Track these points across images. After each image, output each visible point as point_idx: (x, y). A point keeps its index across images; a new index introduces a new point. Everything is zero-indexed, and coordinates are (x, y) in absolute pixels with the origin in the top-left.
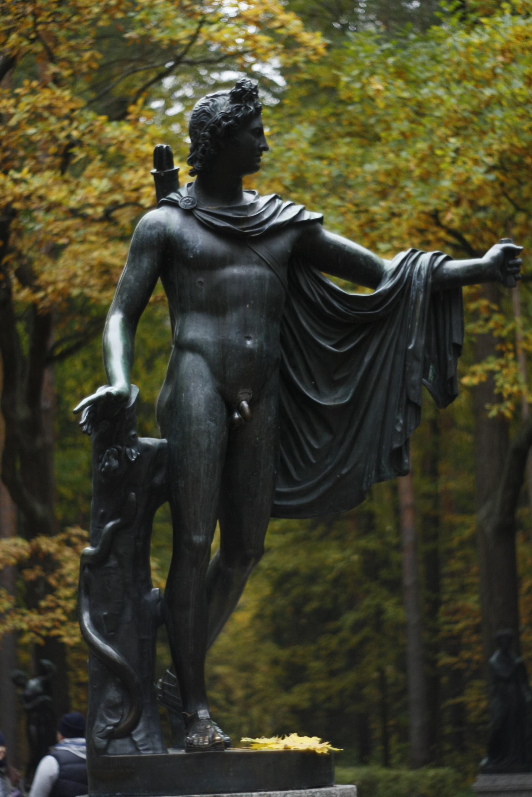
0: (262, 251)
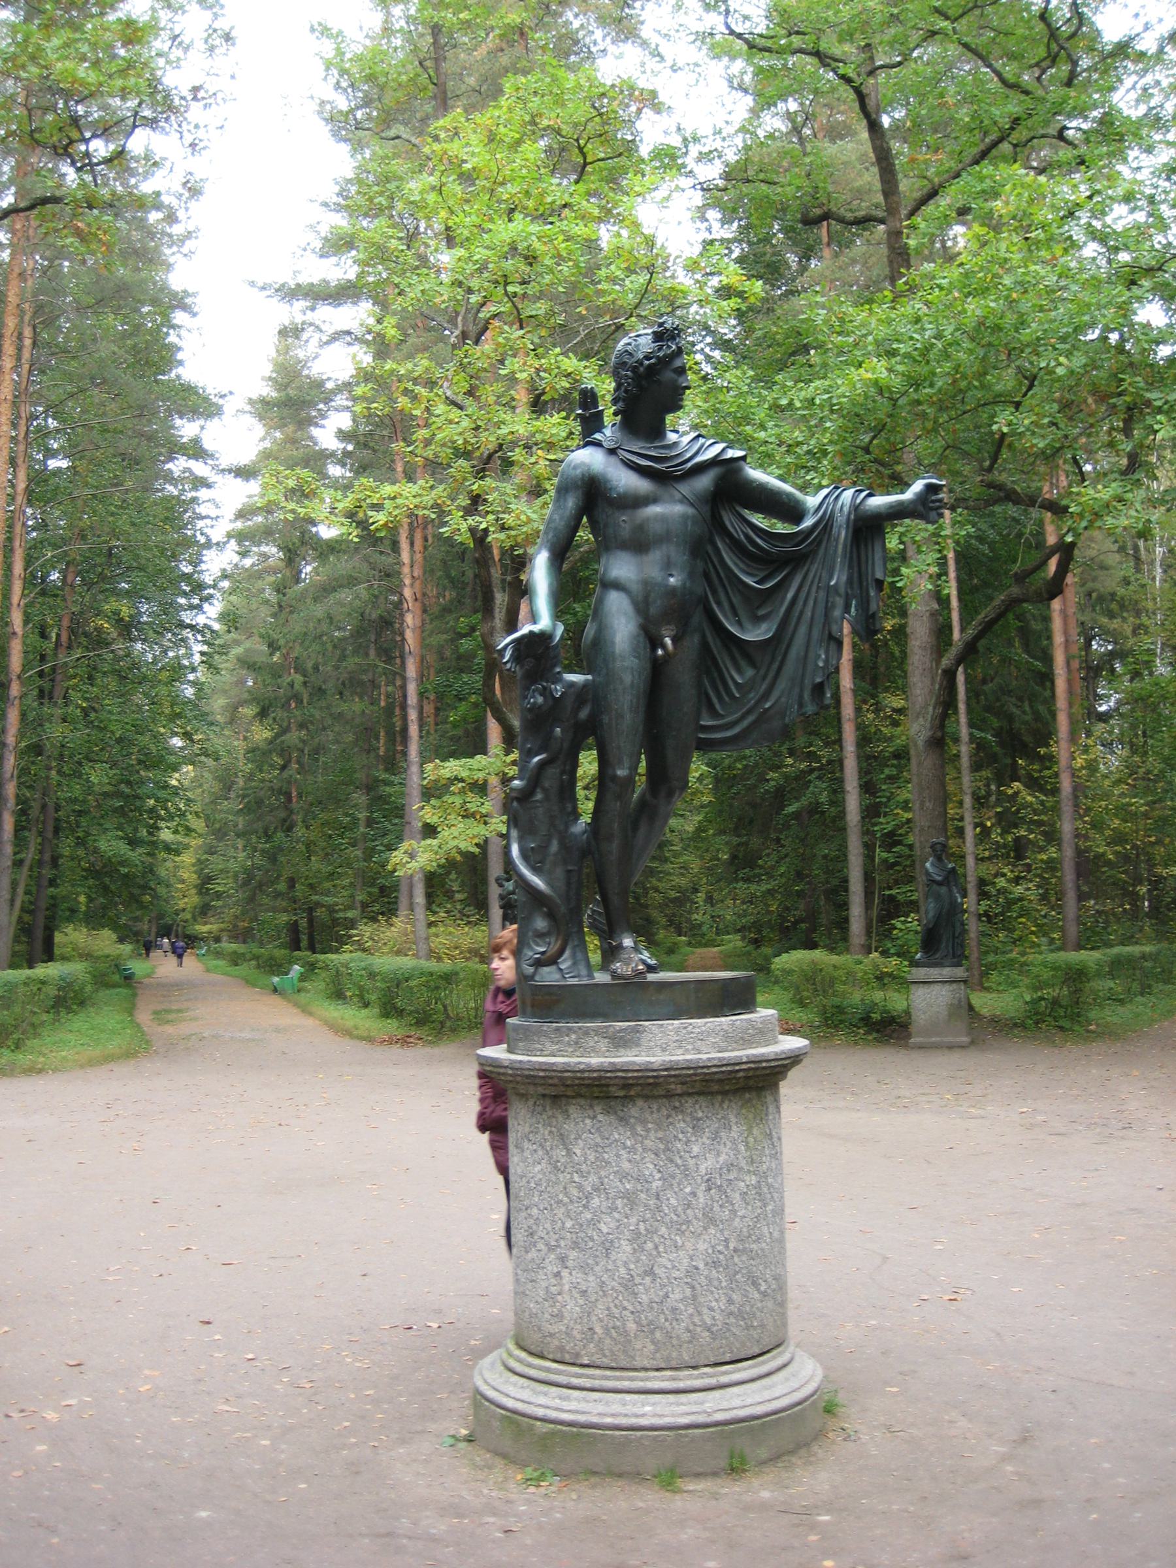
0: (685, 488)
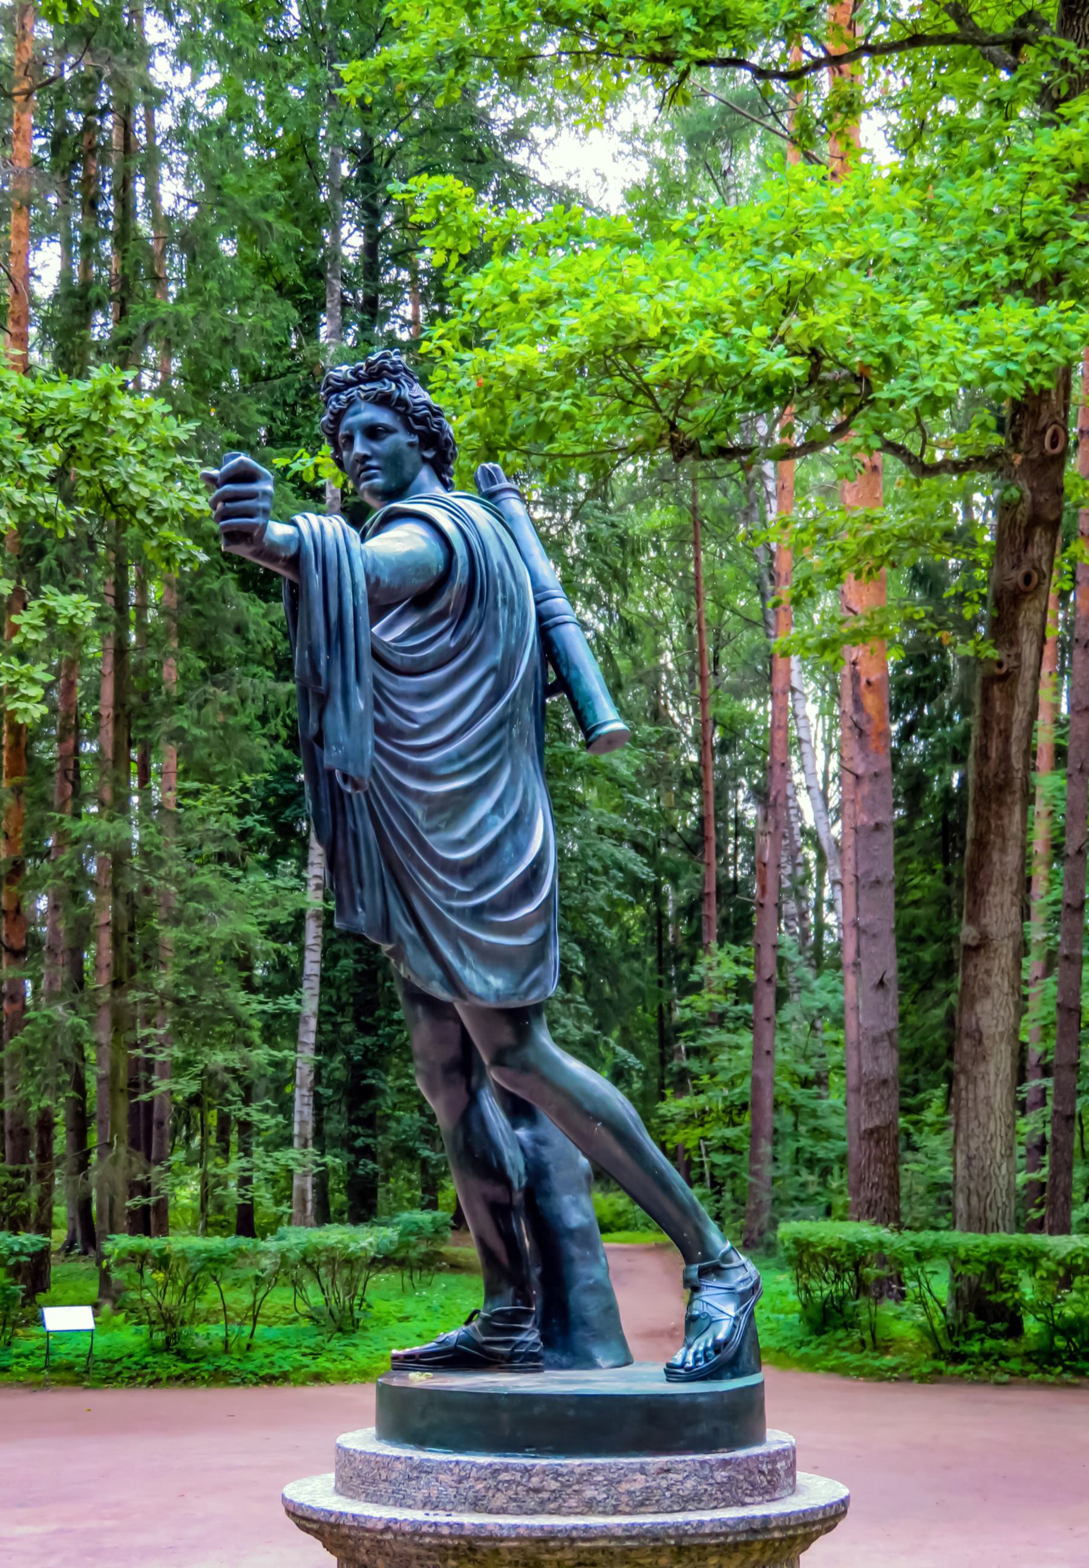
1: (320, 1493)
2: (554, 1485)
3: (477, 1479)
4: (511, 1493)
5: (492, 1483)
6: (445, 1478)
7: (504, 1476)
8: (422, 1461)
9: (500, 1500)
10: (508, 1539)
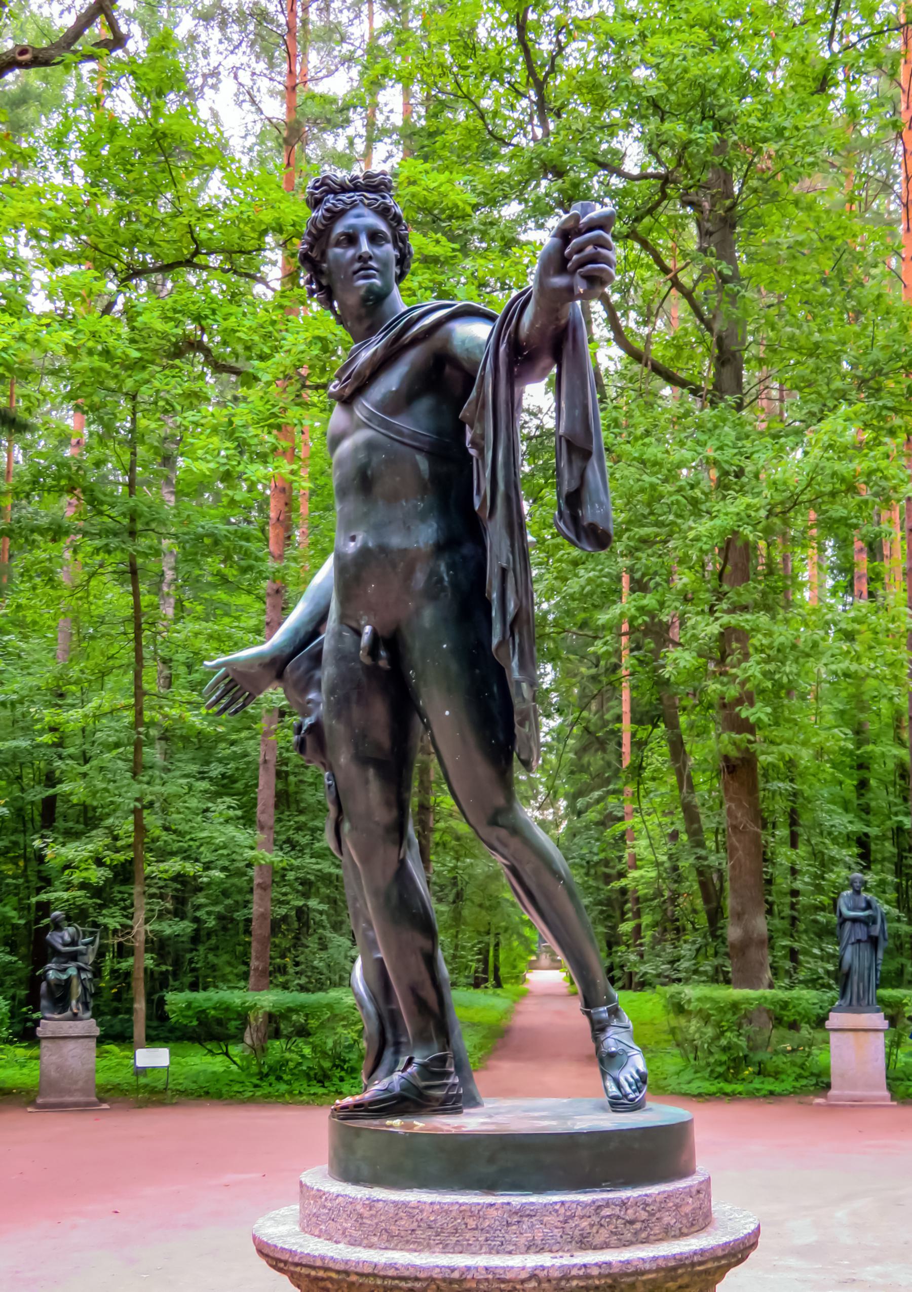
0: (365, 406)
1: (284, 1228)
2: (644, 1215)
3: (582, 1217)
4: (612, 1227)
5: (595, 1219)
6: (551, 1219)
7: (606, 1212)
8: (523, 1205)
9: (604, 1234)
10: (650, 1271)
